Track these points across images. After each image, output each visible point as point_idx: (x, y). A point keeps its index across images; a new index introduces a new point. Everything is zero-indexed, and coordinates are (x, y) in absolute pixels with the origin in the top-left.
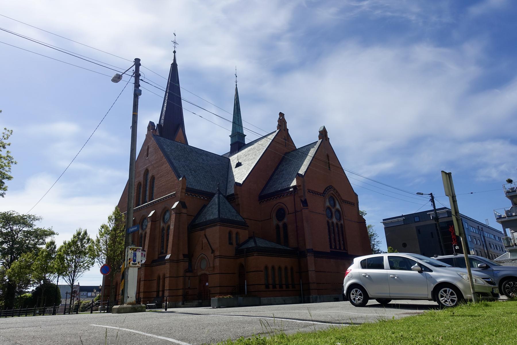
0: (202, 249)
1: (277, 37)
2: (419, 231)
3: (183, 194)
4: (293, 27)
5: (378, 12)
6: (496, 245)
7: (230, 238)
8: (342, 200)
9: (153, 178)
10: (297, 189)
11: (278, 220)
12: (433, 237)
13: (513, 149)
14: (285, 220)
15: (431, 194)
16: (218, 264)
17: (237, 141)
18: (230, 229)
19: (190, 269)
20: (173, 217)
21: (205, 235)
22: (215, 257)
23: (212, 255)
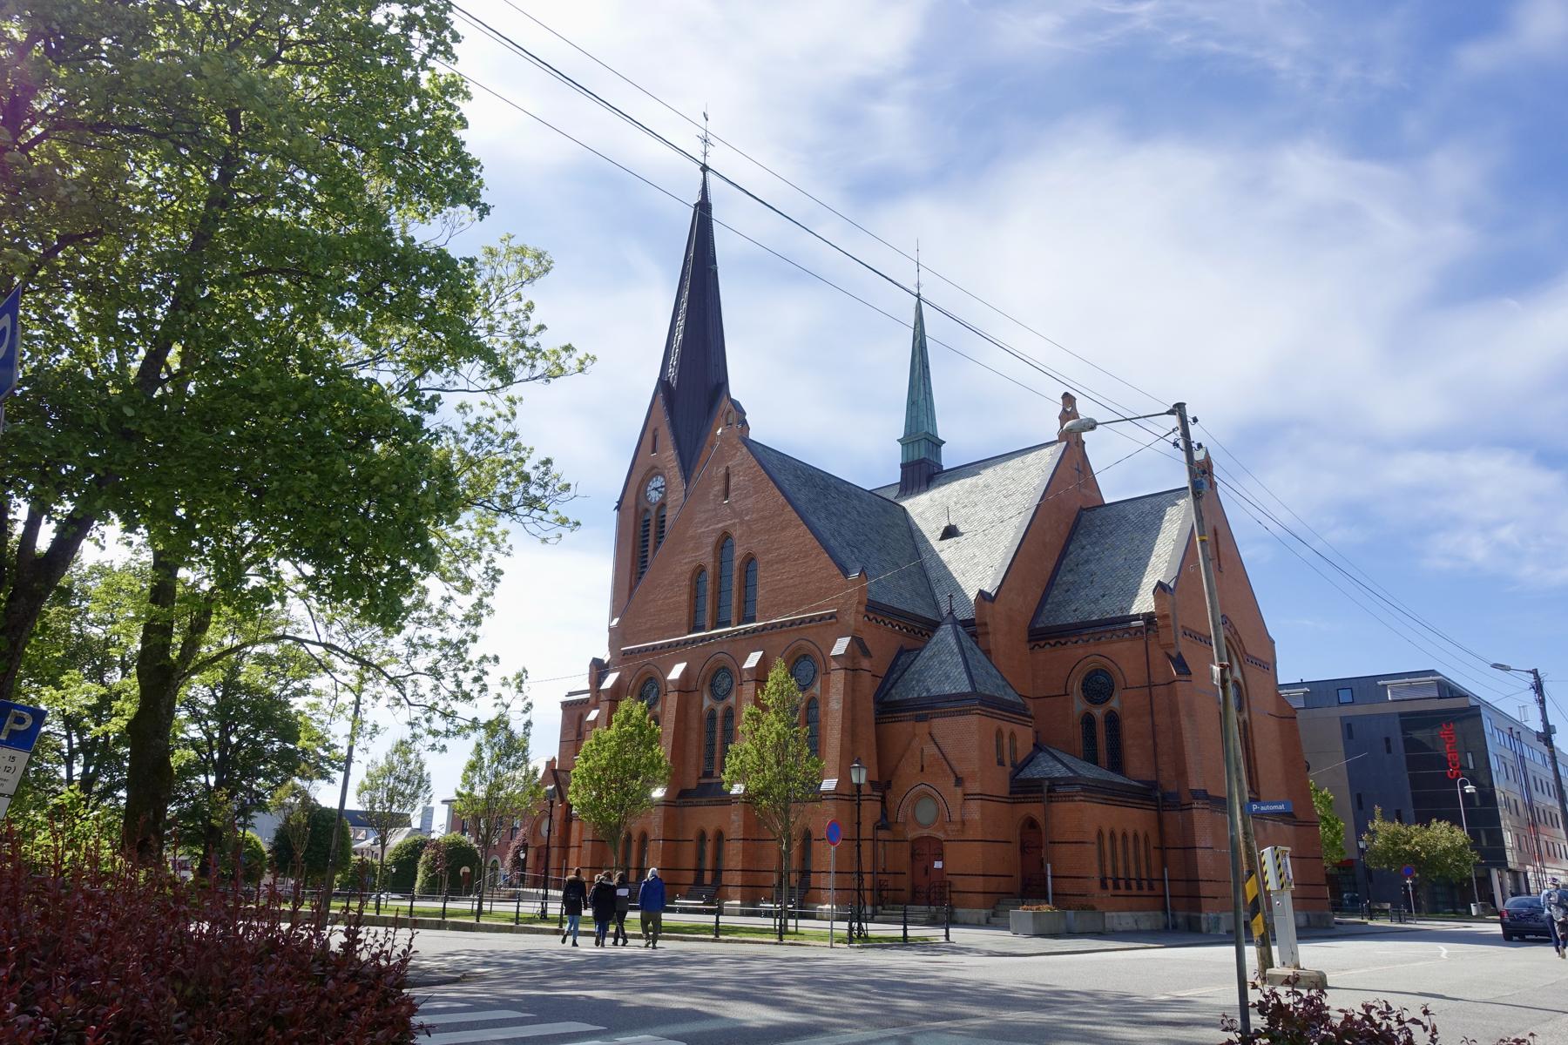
0: (922, 770)
1: (871, 89)
2: (1349, 725)
3: (860, 617)
4: (923, 61)
5: (1181, 38)
6: (1547, 783)
7: (999, 747)
8: (1248, 655)
9: (750, 560)
10: (1155, 624)
11: (1090, 701)
12: (1389, 751)
13: (1547, 481)
14: (1114, 704)
15: (1535, 672)
16: (977, 816)
17: (922, 457)
18: (999, 722)
19: (885, 822)
20: (838, 680)
21: (930, 734)
22: (967, 796)
23: (959, 790)
